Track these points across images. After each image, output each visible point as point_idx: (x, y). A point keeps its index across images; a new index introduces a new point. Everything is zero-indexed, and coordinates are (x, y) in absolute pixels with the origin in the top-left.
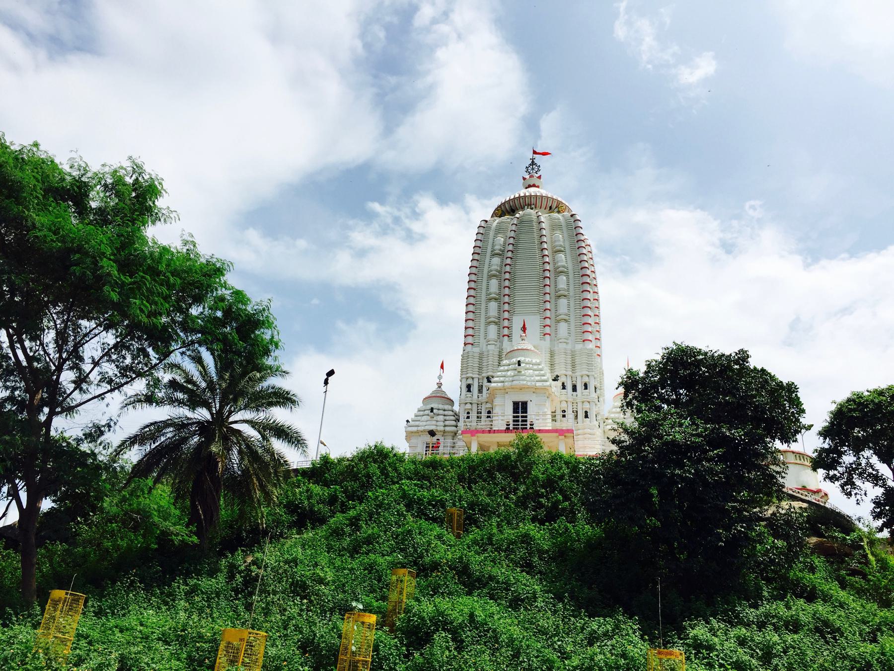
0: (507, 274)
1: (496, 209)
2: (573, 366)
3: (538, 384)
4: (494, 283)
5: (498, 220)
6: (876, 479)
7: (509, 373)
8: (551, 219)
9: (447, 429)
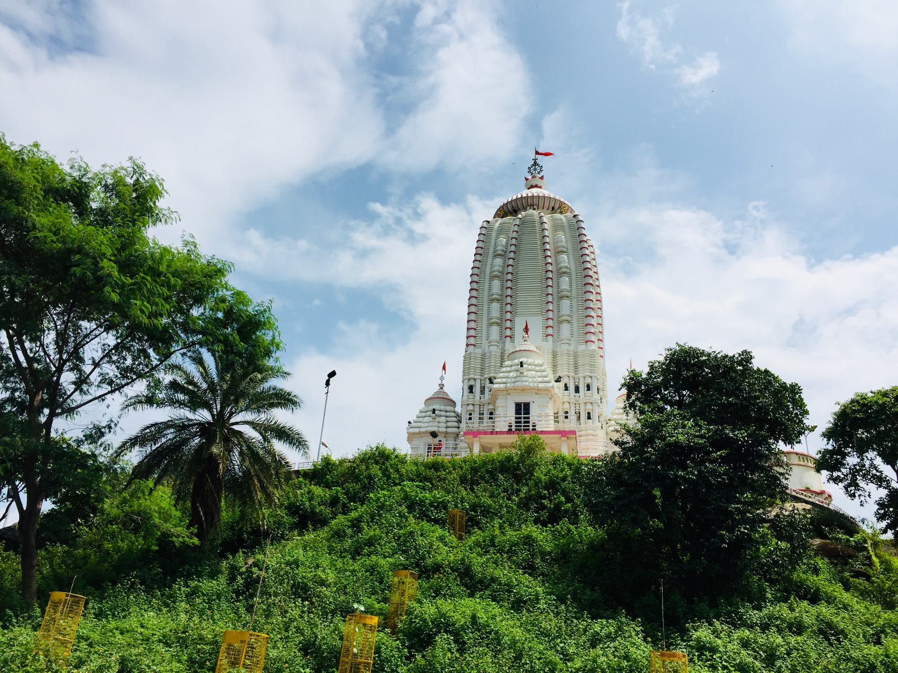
2: (576, 367)
3: (541, 385)
4: (496, 283)
5: (500, 221)
6: (880, 480)
7: (511, 374)
8: (554, 220)
9: (449, 430)
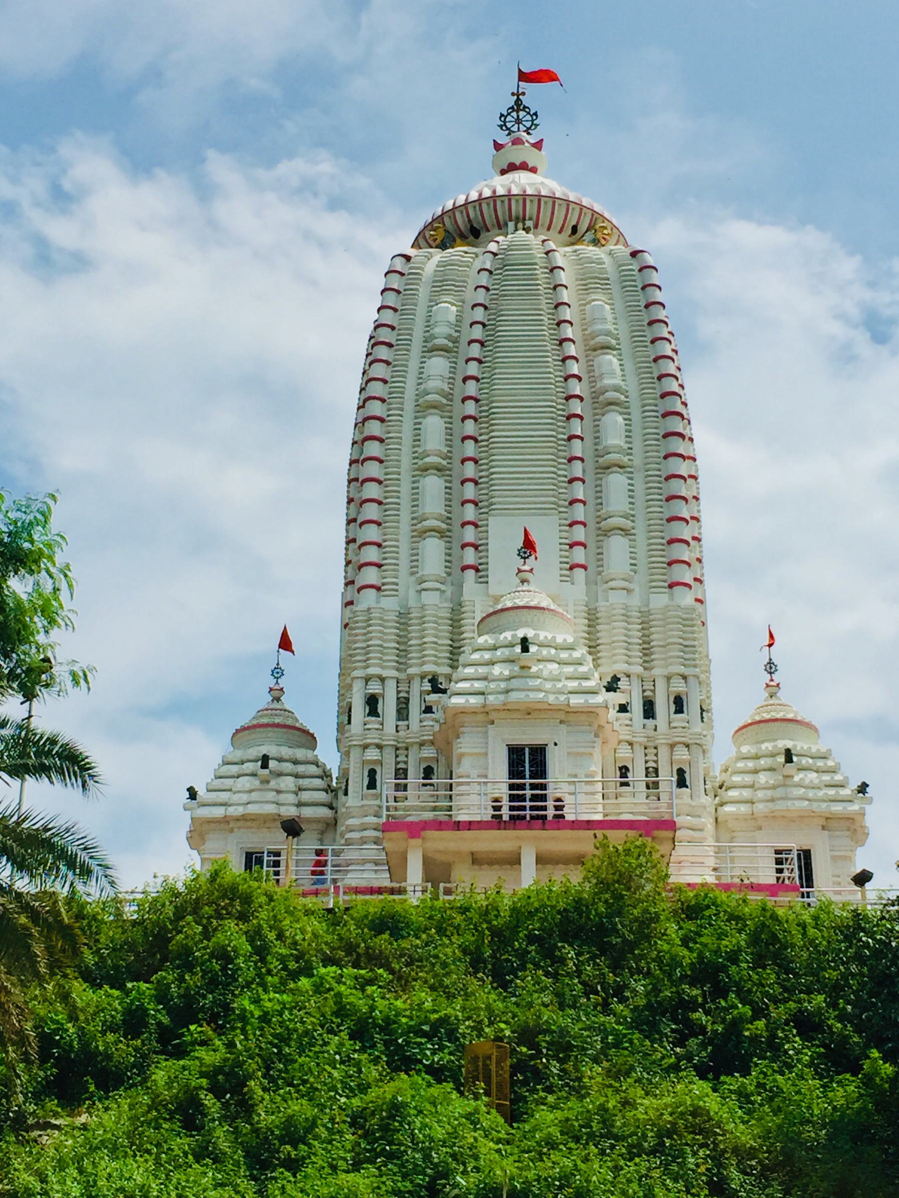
0: (471, 404)
1: (429, 226)
2: (647, 651)
3: (576, 700)
4: (434, 424)
5: (438, 256)
7: (497, 670)
8: (580, 261)
9: (307, 812)
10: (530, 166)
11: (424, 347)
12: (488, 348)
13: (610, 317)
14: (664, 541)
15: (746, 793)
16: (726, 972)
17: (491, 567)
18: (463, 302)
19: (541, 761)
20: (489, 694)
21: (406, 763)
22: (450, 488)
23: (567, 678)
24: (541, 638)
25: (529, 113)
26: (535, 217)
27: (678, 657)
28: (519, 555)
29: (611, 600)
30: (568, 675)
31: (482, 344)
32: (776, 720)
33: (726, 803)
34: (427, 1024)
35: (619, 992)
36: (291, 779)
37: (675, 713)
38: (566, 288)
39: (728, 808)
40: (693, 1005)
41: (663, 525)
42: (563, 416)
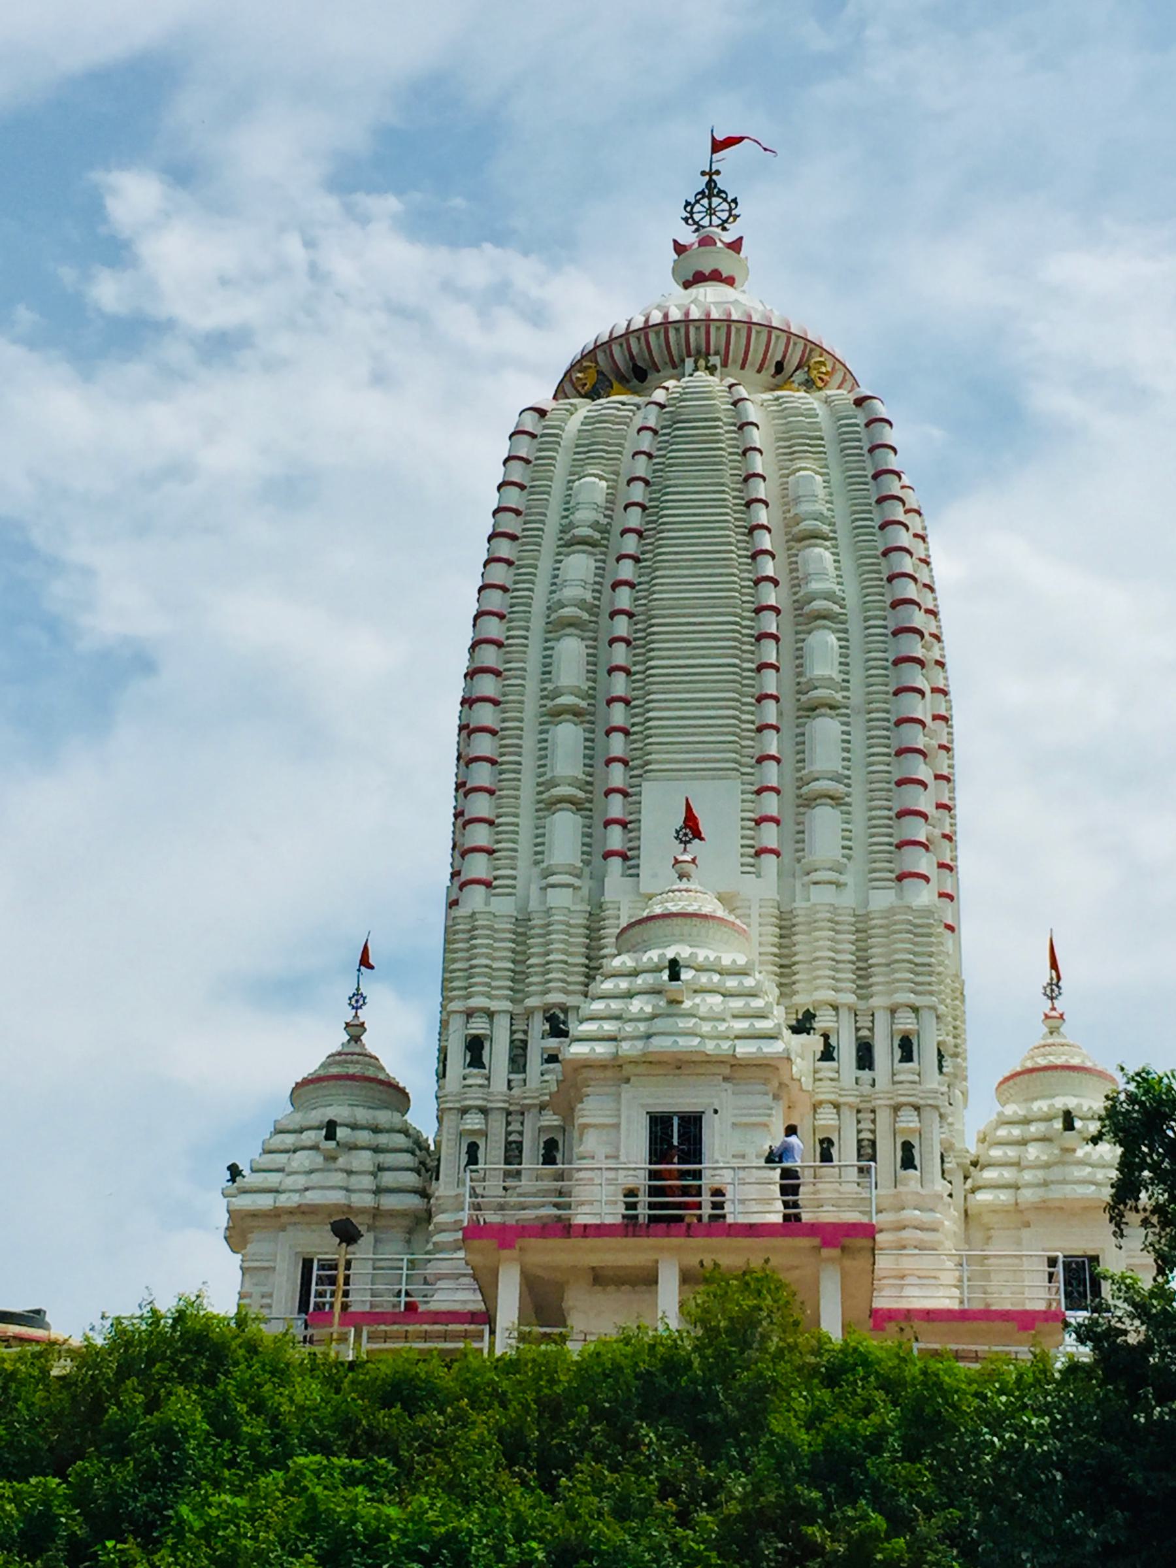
1: (576, 366)
2: (863, 972)
3: (745, 1049)
4: (571, 649)
5: (585, 408)
7: (636, 1006)
8: (783, 411)
9: (390, 1202)
10: (724, 276)
11: (560, 539)
12: (648, 541)
13: (821, 493)
14: (892, 814)
15: (1008, 1174)
16: (861, 1465)
17: (643, 853)
18: (617, 474)
19: (695, 1136)
20: (624, 1039)
21: (521, 1133)
22: (592, 740)
23: (735, 1017)
24: (701, 959)
25: (725, 200)
26: (723, 352)
27: (908, 981)
28: (677, 838)
29: (813, 899)
30: (736, 1012)
31: (640, 534)
32: (1055, 1068)
33: (980, 1188)
34: (427, 1542)
35: (711, 1493)
36: (367, 1154)
37: (901, 1061)
38: (761, 452)
39: (981, 1196)
40: (808, 1514)
41: (890, 790)
42: (752, 636)
